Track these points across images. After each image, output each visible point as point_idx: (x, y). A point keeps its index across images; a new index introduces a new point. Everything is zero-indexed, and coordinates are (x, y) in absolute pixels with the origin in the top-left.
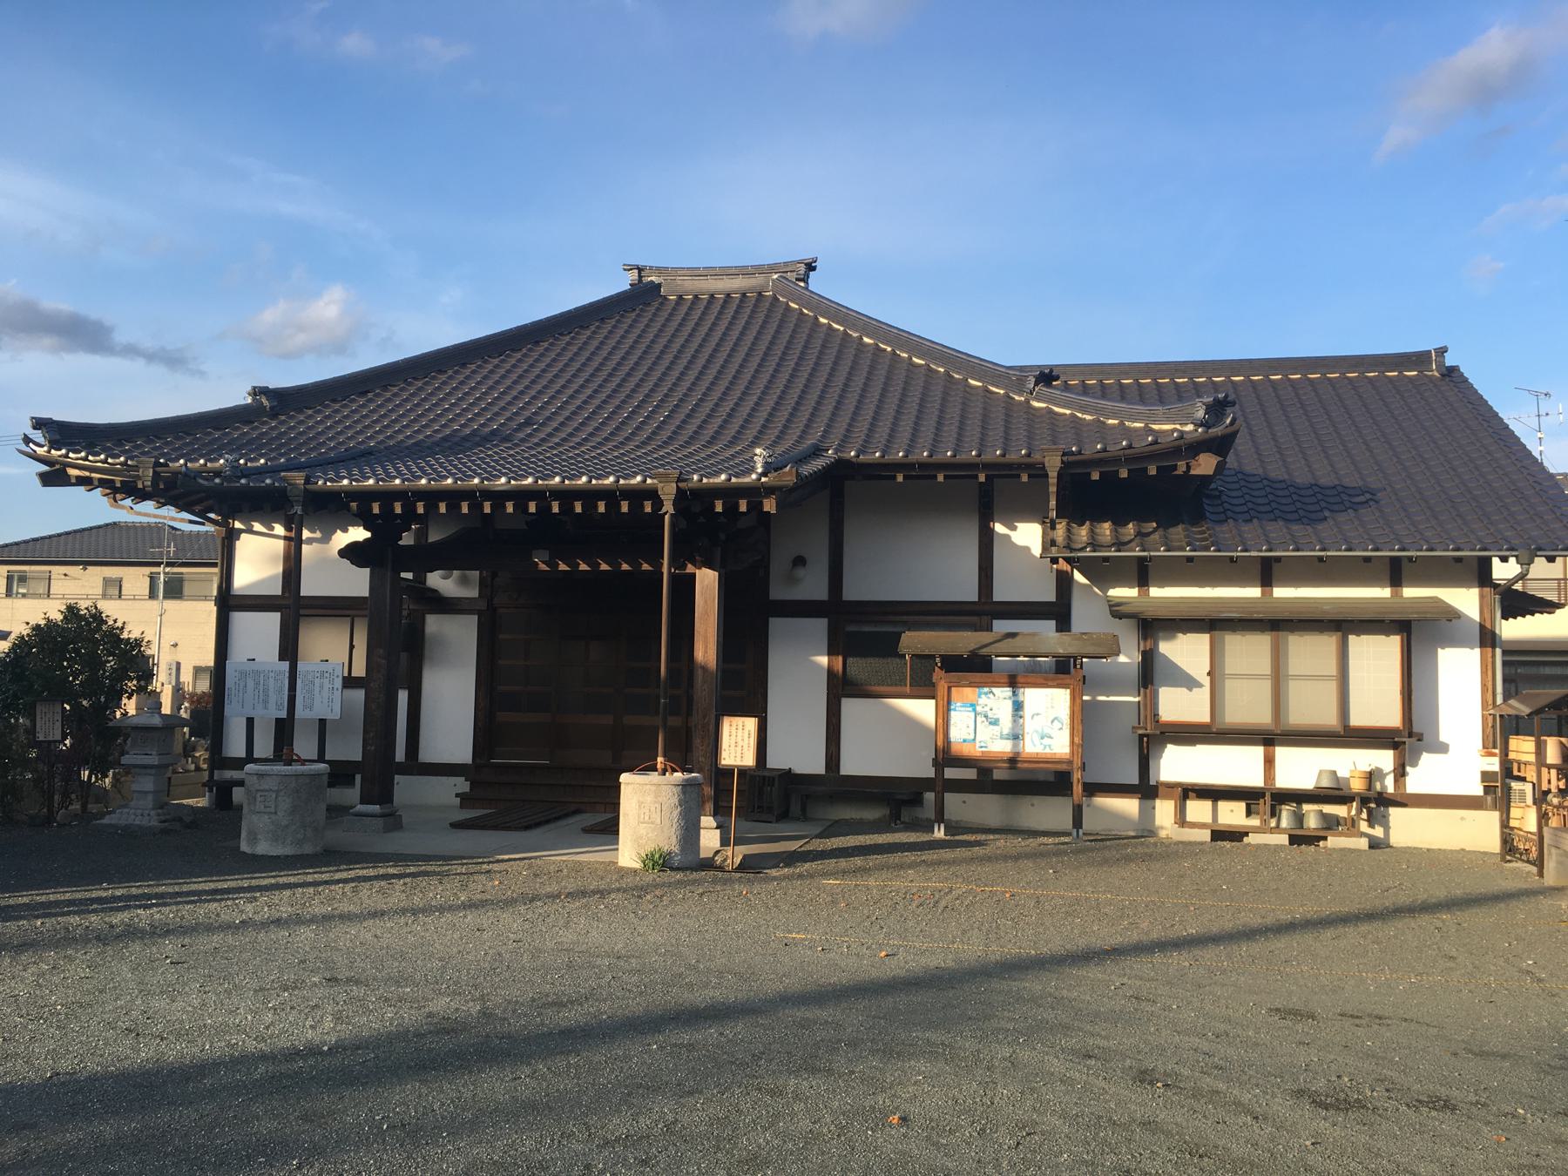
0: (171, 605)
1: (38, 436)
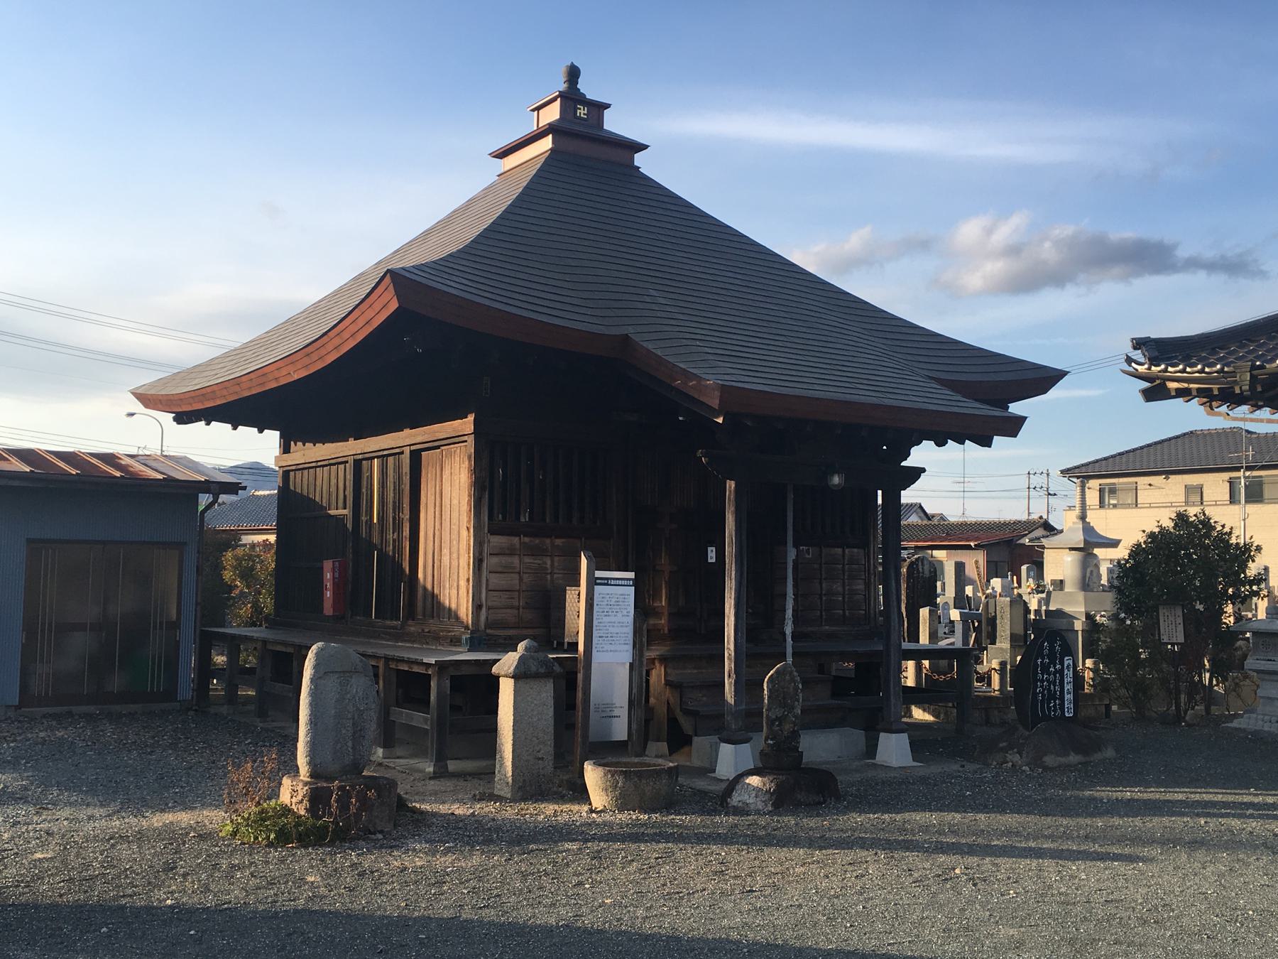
0: (1252, 508)
1: (1137, 355)
